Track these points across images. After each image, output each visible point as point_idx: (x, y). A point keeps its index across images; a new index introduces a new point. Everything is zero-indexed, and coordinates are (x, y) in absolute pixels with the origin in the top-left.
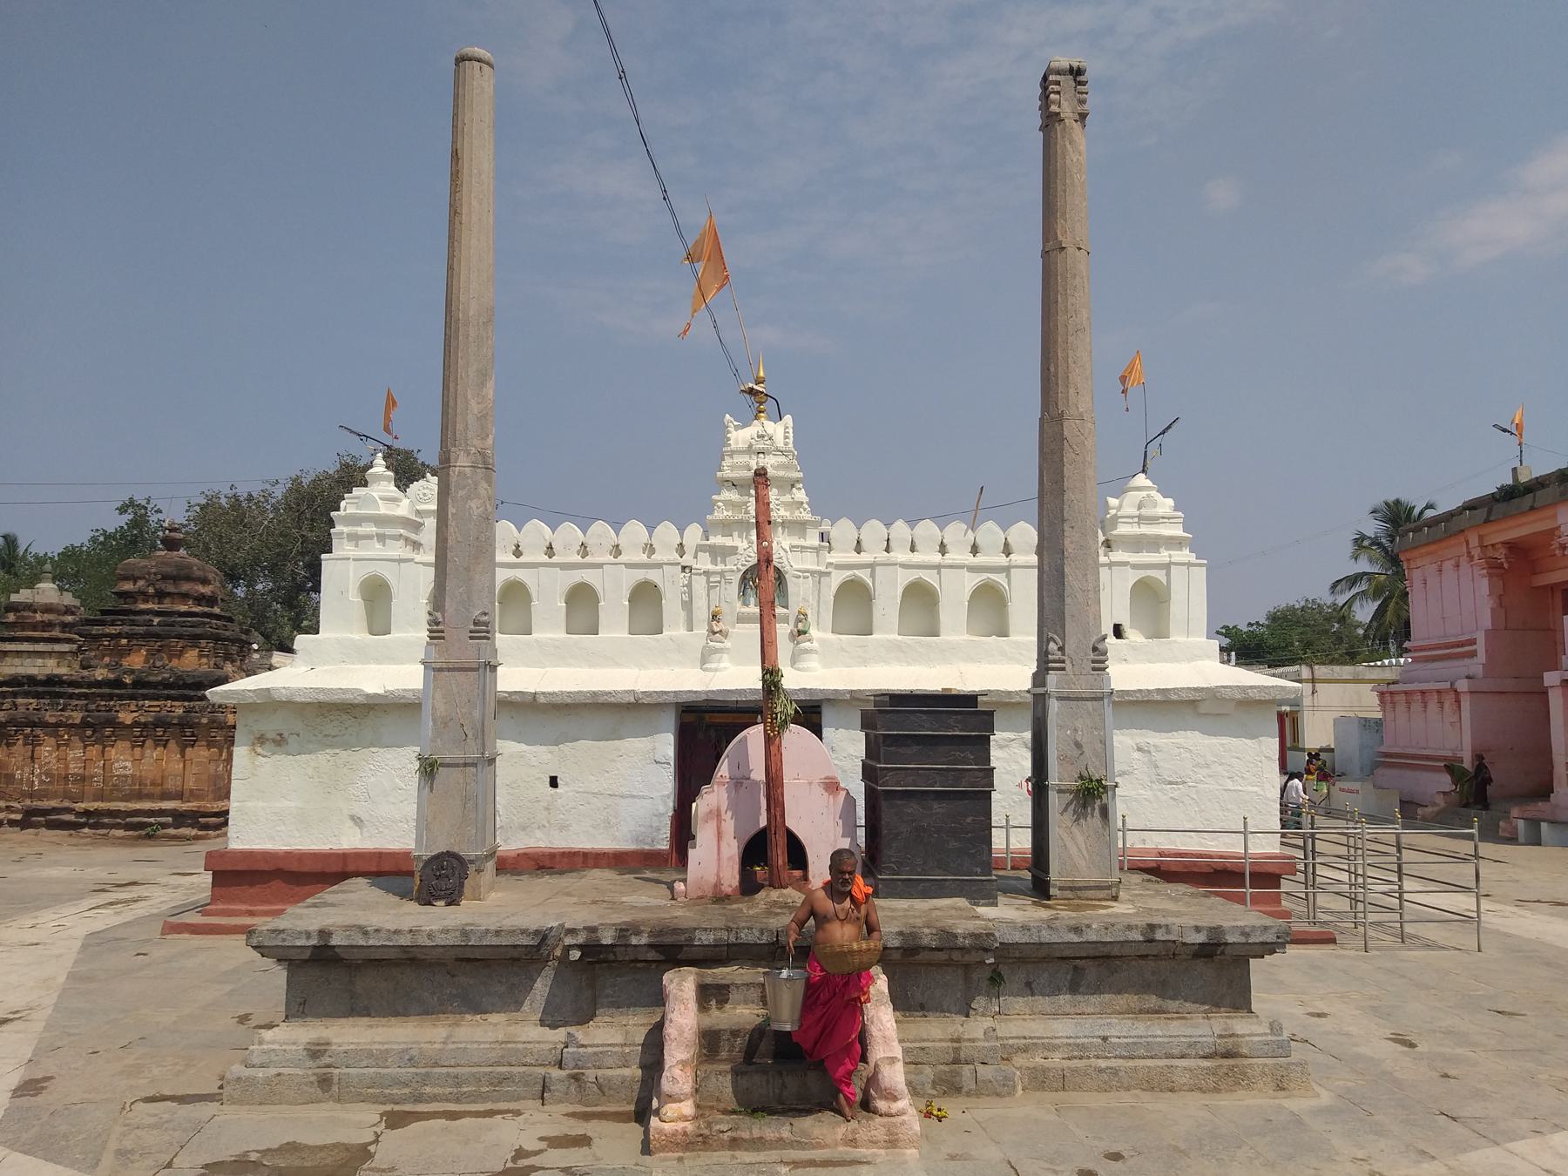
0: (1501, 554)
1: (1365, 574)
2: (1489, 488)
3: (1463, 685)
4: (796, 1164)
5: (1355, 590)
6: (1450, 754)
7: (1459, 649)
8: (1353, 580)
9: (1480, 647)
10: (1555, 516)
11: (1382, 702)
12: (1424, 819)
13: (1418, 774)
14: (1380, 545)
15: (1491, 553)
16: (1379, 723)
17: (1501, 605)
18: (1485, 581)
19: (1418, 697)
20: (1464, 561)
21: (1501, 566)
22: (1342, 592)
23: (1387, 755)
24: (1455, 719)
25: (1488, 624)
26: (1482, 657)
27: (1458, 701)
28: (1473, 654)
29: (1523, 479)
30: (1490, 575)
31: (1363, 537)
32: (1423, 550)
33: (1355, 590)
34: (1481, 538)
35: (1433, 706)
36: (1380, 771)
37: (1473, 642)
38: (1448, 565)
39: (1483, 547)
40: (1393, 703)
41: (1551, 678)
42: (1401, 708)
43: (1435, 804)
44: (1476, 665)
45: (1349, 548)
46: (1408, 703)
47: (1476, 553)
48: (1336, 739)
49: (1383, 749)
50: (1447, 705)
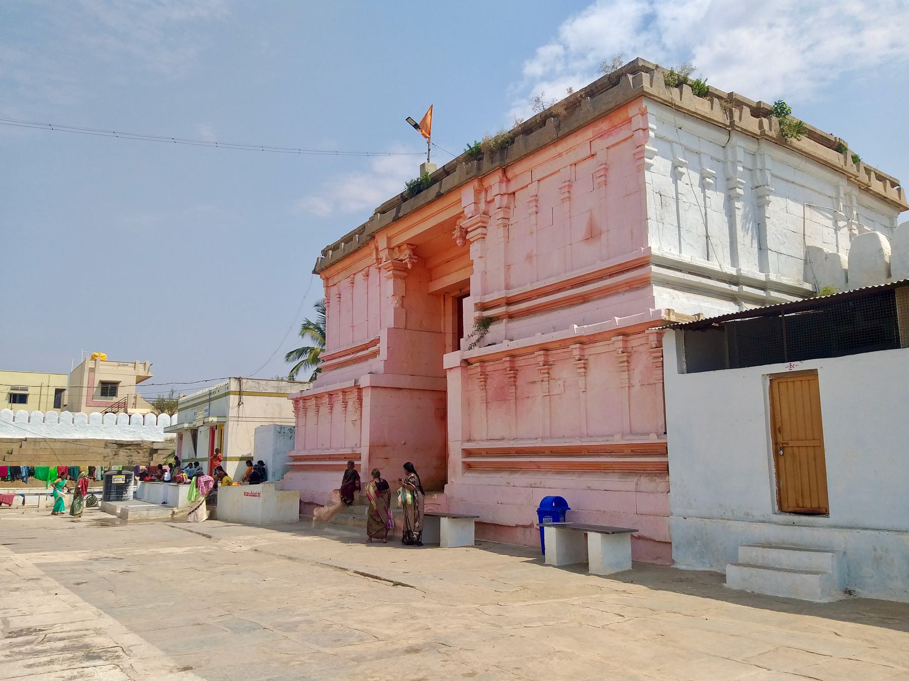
0: (405, 255)
1: (308, 348)
2: (398, 188)
3: (365, 381)
4: (840, 148)
5: (301, 359)
6: (348, 451)
7: (362, 352)
8: (301, 352)
9: (383, 346)
10: (460, 201)
11: (296, 409)
12: (319, 519)
13: (312, 475)
14: (319, 329)
15: (397, 255)
16: (292, 430)
17: (402, 306)
18: (391, 282)
19: (326, 400)
20: (373, 271)
21: (406, 269)
22: (293, 360)
23: (296, 458)
24: (356, 417)
25: (390, 321)
26: (384, 354)
27: (360, 399)
28: (375, 354)
29: (431, 170)
30: (395, 277)
31: (309, 323)
32: (339, 266)
33: (301, 359)
34: (389, 239)
35: (338, 407)
36: (289, 475)
37: (376, 342)
38: (360, 277)
39: (391, 249)
40: (305, 408)
41: (451, 359)
42: (311, 413)
43: (330, 503)
44: (378, 364)
45: (299, 328)
46: (317, 406)
47: (384, 255)
48: (256, 447)
49: (293, 453)
50: (350, 403)
